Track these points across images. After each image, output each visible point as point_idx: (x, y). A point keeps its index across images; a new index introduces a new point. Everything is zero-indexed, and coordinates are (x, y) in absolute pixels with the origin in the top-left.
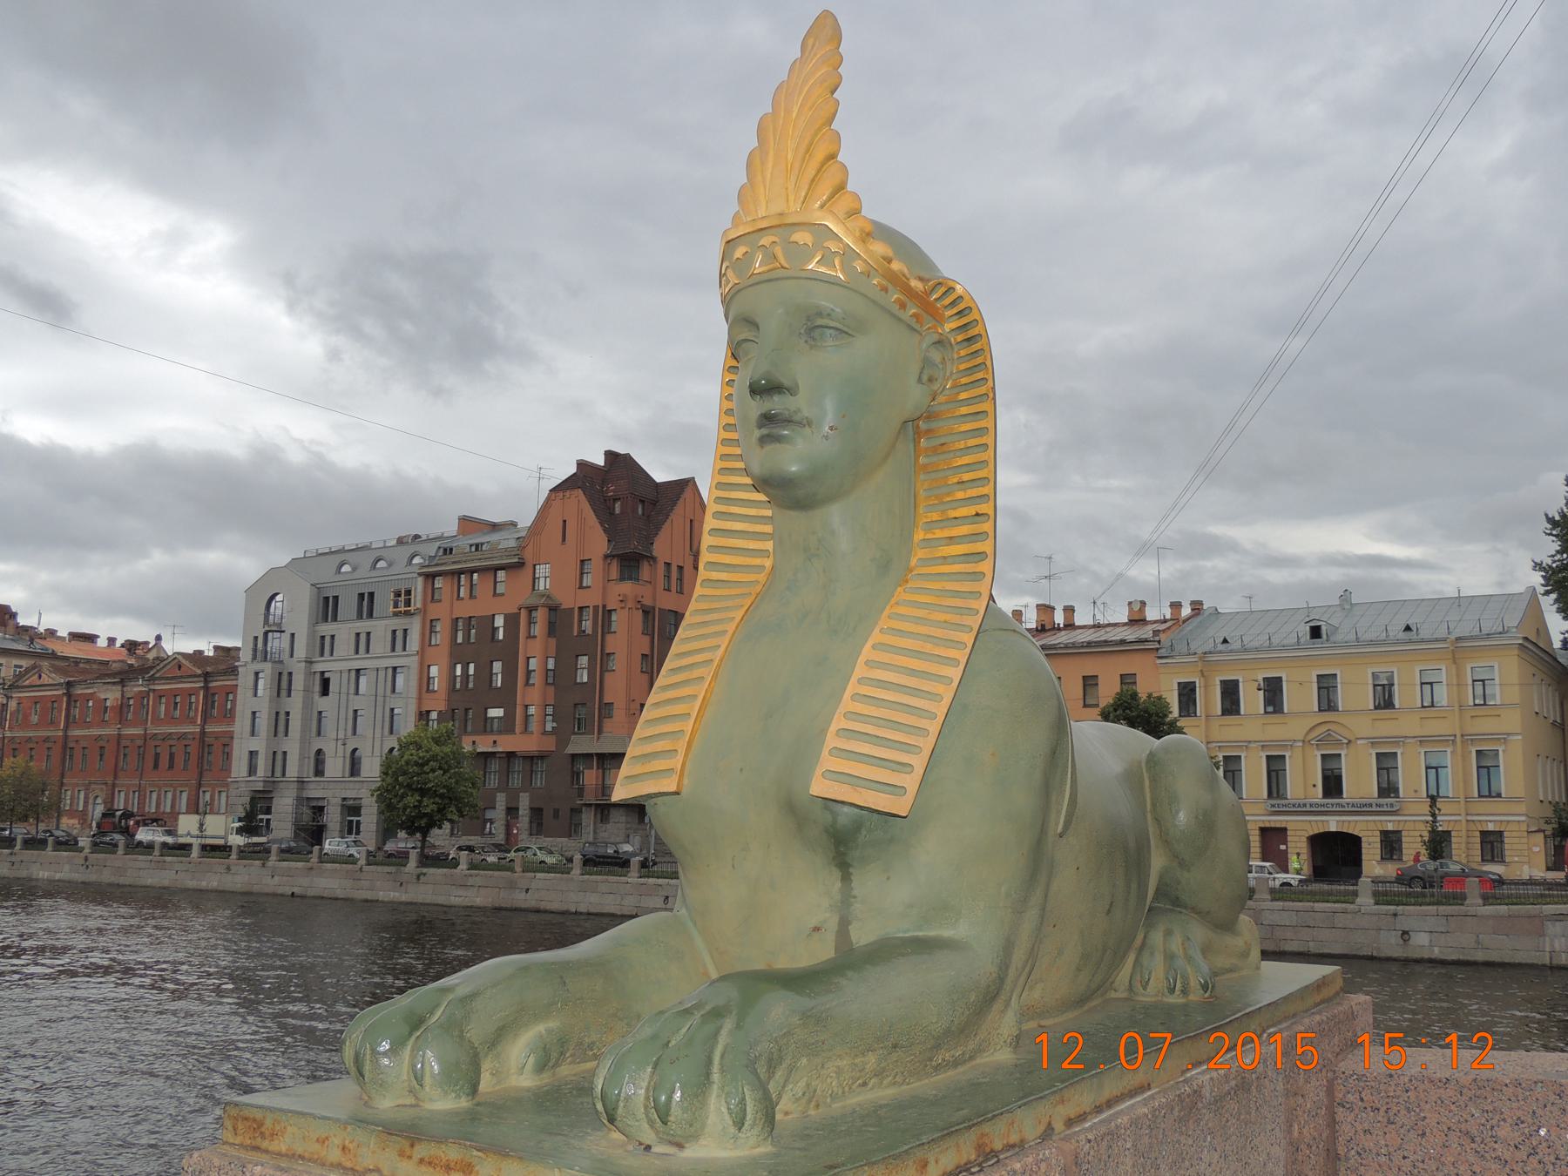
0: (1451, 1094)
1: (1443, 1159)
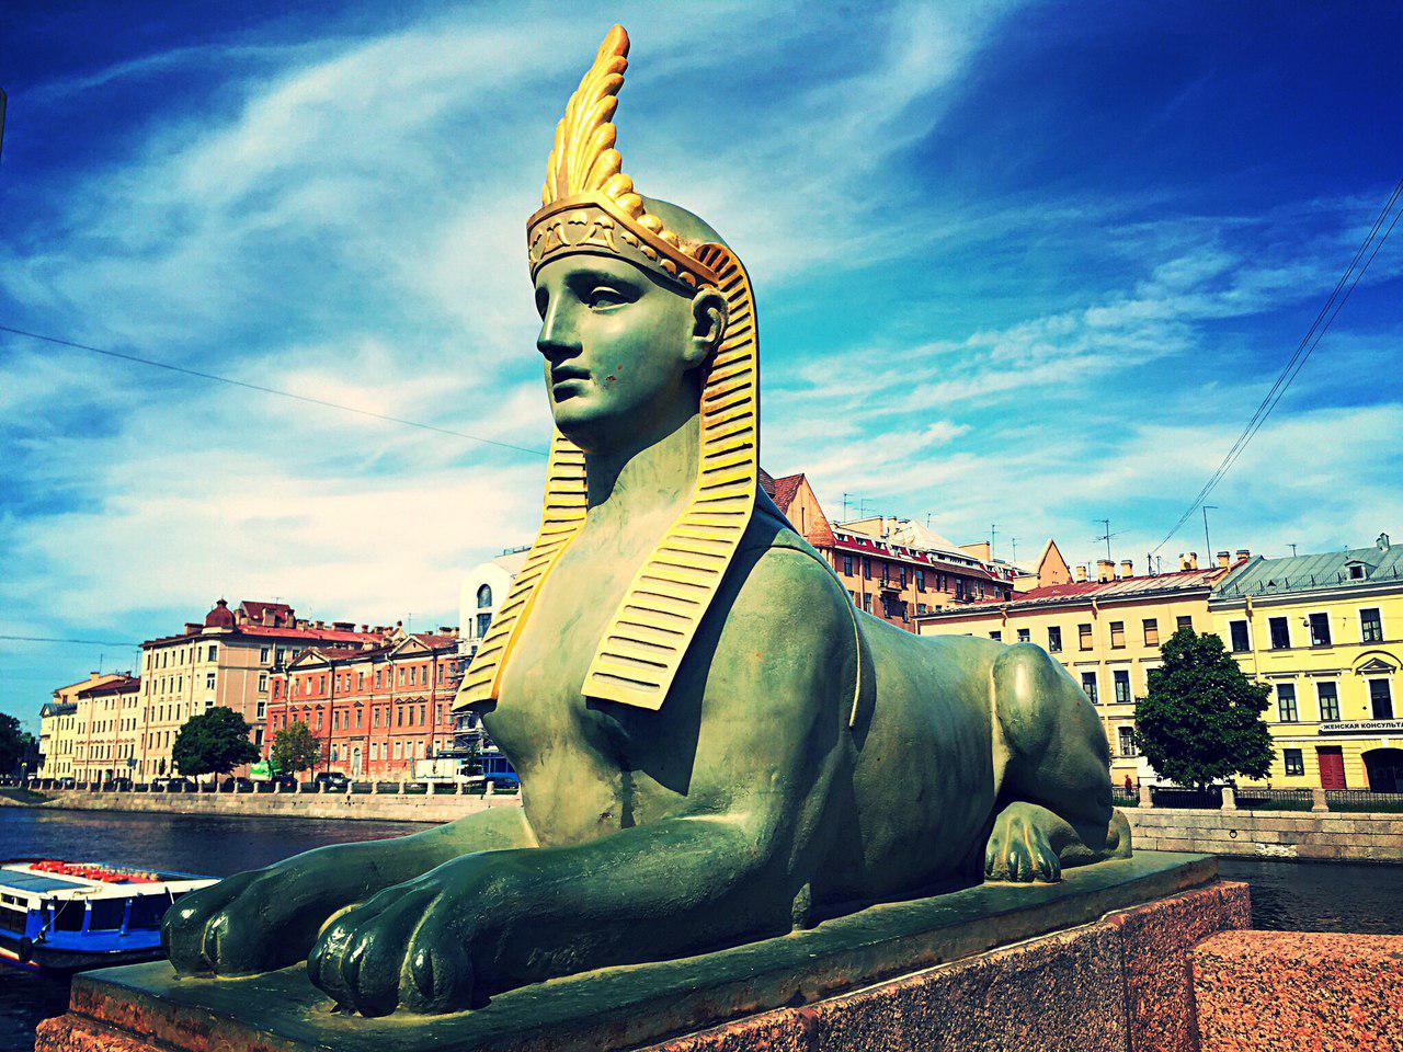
0: (1302, 975)
1: (1297, 1038)
